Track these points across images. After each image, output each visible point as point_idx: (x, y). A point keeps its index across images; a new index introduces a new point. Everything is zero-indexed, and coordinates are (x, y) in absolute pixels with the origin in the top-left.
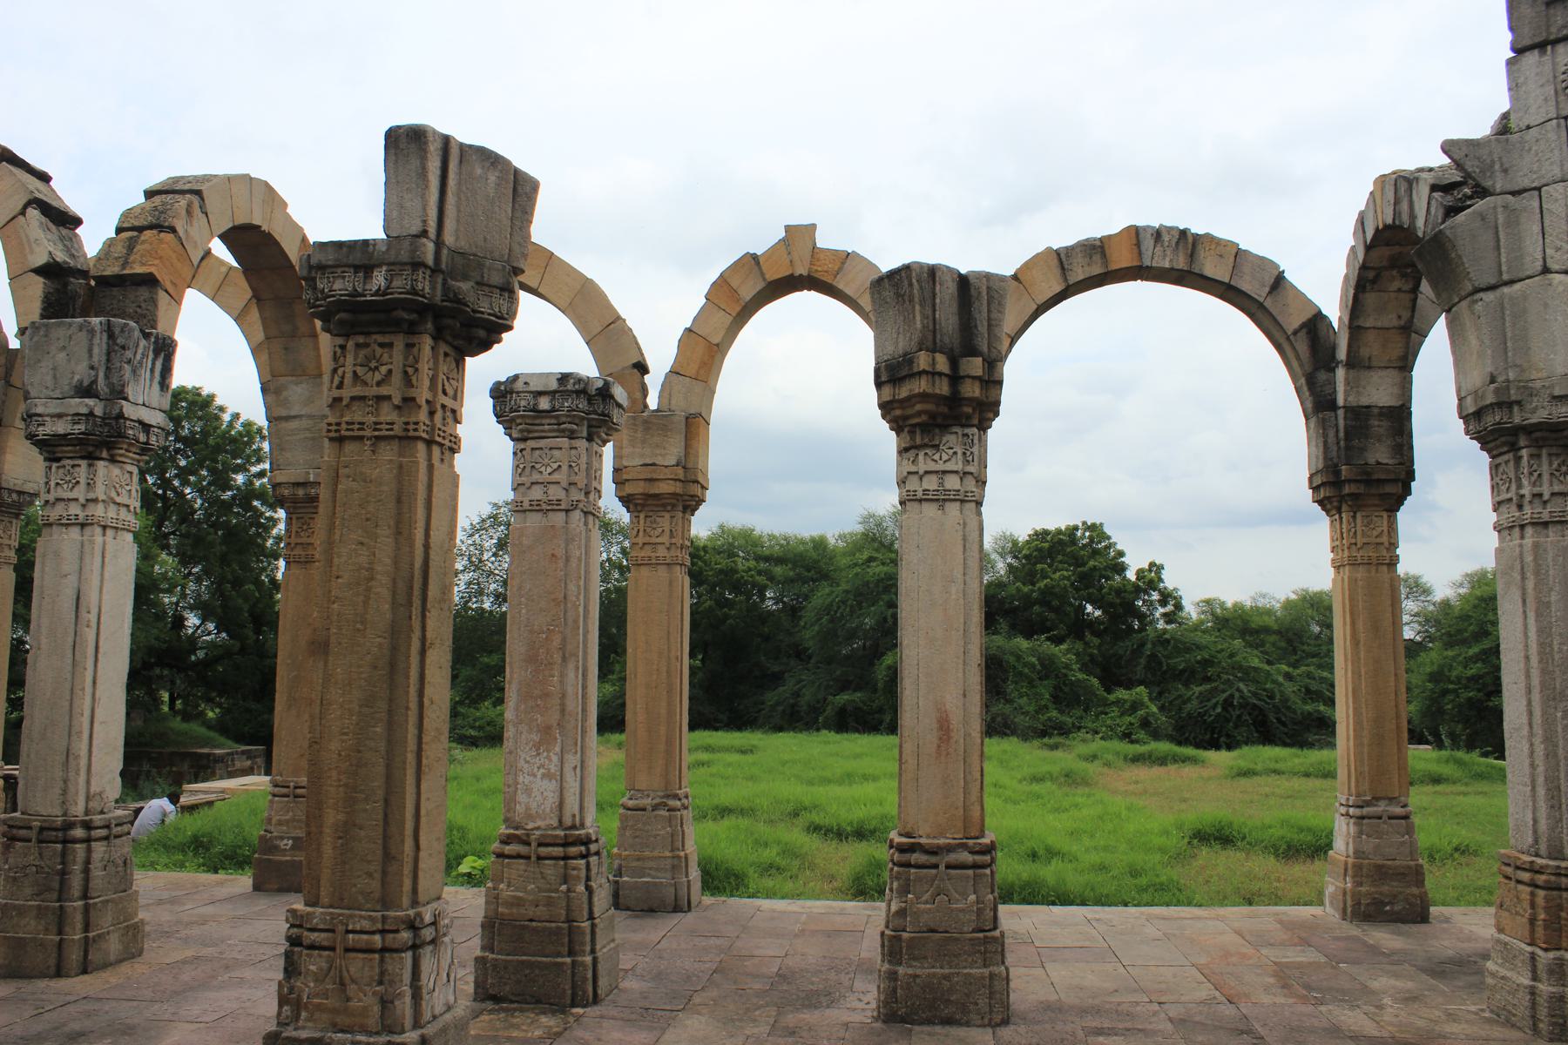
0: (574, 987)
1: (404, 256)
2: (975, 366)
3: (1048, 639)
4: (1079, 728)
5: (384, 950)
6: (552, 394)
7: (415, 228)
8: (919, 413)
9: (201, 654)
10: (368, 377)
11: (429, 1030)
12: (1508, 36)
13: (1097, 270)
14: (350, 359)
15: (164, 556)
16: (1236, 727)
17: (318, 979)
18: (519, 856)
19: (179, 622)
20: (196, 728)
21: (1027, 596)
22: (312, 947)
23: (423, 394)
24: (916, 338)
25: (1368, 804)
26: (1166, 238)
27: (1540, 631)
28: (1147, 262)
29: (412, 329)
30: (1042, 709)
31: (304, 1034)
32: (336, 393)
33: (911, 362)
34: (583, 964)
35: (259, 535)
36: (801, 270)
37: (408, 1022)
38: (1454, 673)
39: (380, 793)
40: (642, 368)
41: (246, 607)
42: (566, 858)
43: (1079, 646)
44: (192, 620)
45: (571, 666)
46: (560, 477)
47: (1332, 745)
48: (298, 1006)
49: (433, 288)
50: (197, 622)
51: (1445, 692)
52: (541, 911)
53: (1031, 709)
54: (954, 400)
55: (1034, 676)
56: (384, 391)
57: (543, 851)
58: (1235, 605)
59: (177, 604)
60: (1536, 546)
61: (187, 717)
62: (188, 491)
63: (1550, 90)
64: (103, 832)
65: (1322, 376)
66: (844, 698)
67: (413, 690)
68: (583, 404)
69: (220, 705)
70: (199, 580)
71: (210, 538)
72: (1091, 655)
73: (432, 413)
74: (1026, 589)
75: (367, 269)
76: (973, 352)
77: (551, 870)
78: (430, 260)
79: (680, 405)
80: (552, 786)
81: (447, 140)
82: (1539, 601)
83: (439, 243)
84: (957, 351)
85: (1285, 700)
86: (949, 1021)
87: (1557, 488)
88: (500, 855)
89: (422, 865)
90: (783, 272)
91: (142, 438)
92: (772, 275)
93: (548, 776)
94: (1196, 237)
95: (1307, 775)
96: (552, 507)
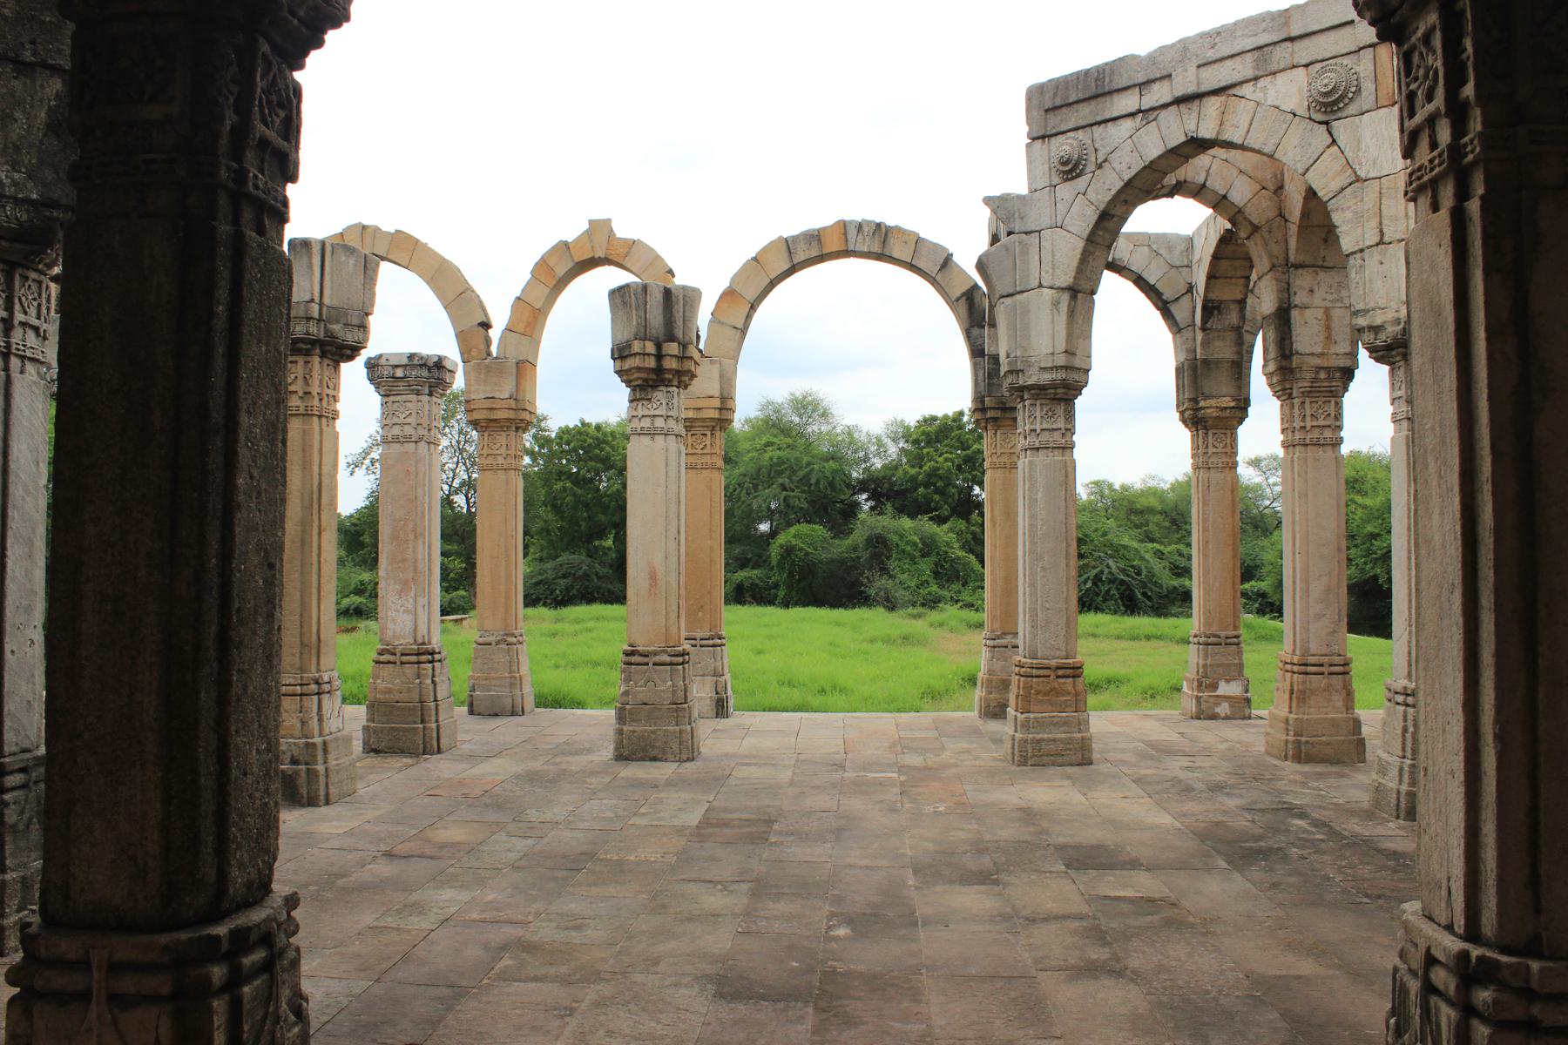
2: (672, 348)
3: (931, 519)
6: (405, 366)
7: (307, 298)
12: (1026, 129)
13: (814, 253)
16: (1105, 601)
21: (913, 479)
23: (315, 390)
24: (634, 330)
25: (999, 637)
26: (866, 229)
27: (1031, 517)
28: (851, 248)
29: (308, 353)
36: (600, 254)
37: (316, 732)
40: (486, 325)
43: (962, 524)
47: (1190, 616)
52: (404, 697)
53: (913, 584)
54: (659, 370)
55: (917, 554)
57: (405, 658)
58: (1123, 487)
65: (976, 331)
66: (741, 575)
68: (425, 373)
74: (913, 471)
76: (671, 338)
80: (410, 617)
83: (321, 304)
84: (662, 338)
85: (1151, 575)
86: (654, 759)
88: (377, 662)
90: (587, 256)
92: (579, 257)
93: (407, 611)
94: (888, 229)
95: (1118, 638)
96: (406, 439)
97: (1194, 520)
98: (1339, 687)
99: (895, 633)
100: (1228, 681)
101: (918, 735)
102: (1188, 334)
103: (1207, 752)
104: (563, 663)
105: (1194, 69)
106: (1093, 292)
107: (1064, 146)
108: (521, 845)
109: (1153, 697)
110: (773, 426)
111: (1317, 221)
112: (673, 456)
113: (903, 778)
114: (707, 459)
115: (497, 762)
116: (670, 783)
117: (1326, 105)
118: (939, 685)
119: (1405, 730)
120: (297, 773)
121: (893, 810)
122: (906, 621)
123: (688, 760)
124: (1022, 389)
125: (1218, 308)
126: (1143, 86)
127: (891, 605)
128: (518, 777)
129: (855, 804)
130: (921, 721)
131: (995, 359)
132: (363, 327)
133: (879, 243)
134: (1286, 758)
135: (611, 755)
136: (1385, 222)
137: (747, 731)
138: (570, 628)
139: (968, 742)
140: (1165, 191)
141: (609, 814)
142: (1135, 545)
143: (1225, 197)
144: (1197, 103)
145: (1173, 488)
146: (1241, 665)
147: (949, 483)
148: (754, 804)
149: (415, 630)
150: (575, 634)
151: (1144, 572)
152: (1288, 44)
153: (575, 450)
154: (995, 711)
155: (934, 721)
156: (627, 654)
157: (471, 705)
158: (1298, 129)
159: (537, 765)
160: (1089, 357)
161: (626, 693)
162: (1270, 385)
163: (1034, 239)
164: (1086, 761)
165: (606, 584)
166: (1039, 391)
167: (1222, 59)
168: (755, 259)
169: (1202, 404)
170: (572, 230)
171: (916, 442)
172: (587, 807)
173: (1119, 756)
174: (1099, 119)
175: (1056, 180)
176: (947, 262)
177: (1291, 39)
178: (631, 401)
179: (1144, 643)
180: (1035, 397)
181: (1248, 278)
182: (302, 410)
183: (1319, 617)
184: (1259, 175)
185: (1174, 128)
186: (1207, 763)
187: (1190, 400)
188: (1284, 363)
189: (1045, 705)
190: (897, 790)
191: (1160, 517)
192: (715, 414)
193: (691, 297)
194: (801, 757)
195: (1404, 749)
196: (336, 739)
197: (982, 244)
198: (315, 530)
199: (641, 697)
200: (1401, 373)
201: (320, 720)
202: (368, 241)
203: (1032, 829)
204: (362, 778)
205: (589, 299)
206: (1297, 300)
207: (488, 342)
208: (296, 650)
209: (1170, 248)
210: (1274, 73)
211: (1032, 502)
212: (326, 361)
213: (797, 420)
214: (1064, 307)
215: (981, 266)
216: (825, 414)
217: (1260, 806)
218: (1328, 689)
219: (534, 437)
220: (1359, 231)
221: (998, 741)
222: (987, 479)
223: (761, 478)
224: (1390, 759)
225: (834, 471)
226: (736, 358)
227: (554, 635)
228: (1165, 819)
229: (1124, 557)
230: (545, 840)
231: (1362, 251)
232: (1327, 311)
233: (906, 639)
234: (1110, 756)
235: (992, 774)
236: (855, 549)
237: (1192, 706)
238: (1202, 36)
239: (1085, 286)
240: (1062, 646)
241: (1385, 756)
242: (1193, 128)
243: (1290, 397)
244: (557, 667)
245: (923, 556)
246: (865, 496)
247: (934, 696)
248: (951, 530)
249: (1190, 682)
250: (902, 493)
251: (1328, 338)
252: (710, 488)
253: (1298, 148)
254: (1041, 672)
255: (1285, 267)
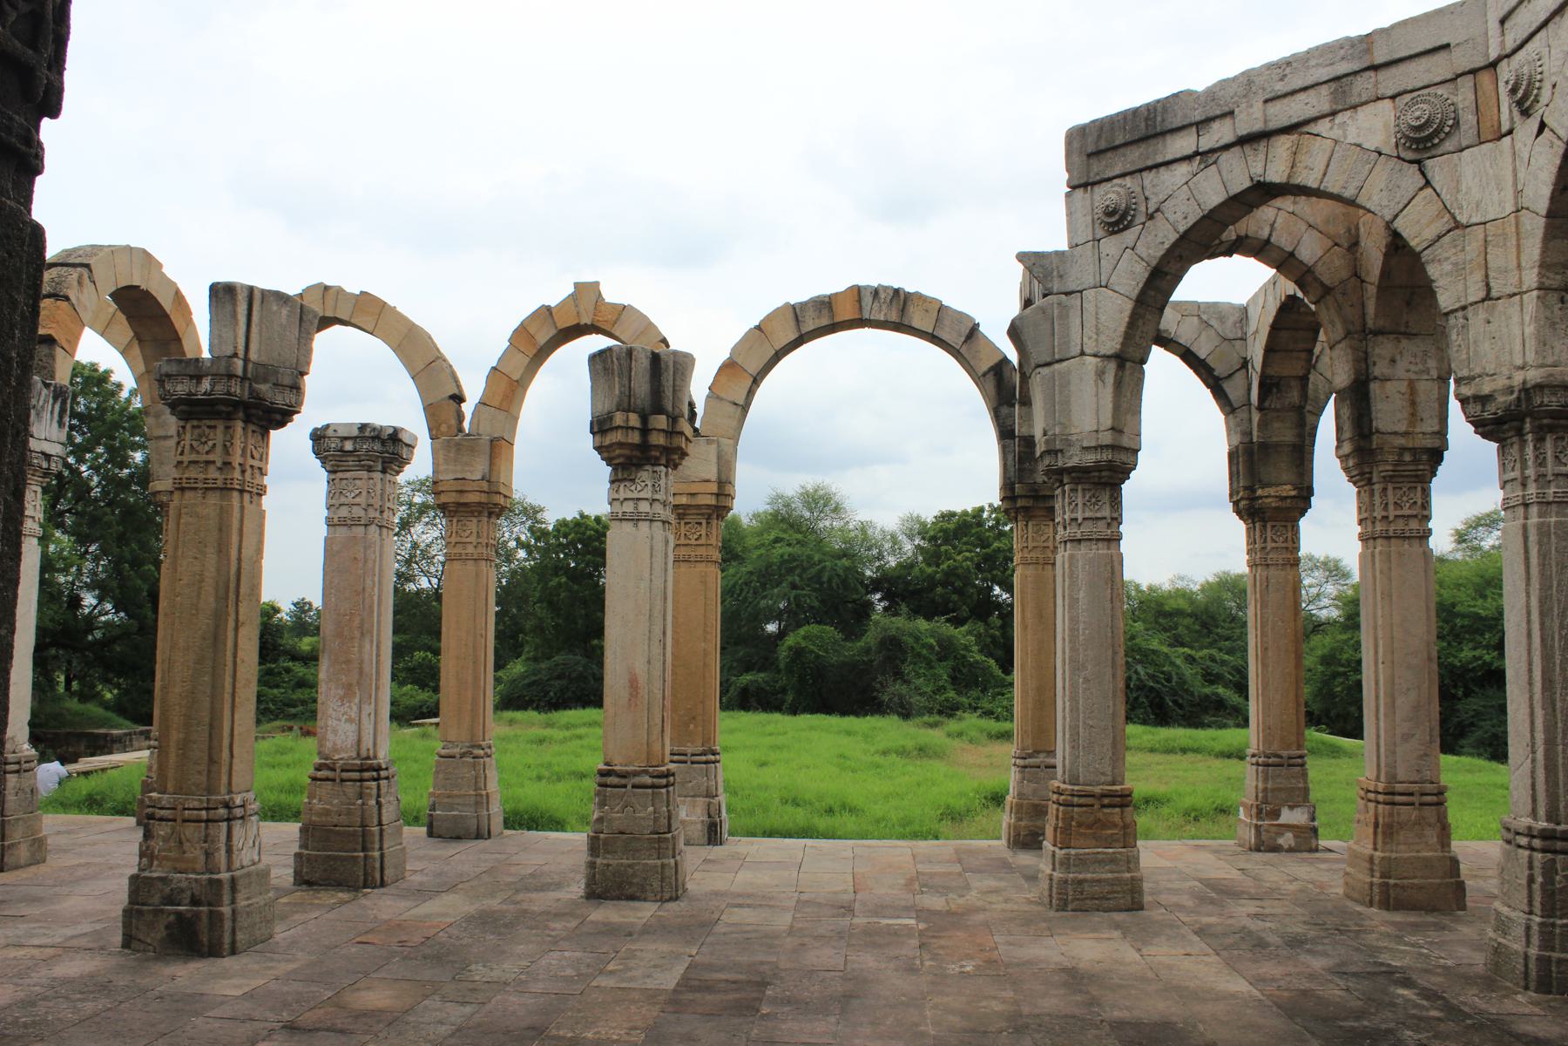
0: (365, 874)
1: (222, 371)
2: (660, 421)
3: (948, 620)
4: (975, 709)
5: (208, 821)
6: (354, 438)
7: (229, 352)
8: (619, 456)
9: (98, 634)
10: (200, 448)
11: (237, 873)
12: (1066, 176)
13: (825, 322)
14: (188, 436)
15: (58, 534)
17: (166, 840)
18: (327, 779)
19: (75, 602)
20: (93, 709)
21: (931, 578)
22: (161, 819)
23: (237, 459)
25: (1030, 756)
27: (1071, 619)
28: (866, 316)
29: (229, 417)
30: (940, 690)
31: (155, 875)
32: (179, 458)
33: (611, 419)
34: (373, 858)
35: (157, 513)
37: (223, 866)
38: (1345, 656)
39: (207, 720)
40: (459, 398)
41: (146, 587)
42: (361, 780)
44: (89, 600)
45: (367, 640)
46: (361, 500)
48: (152, 857)
49: (242, 389)
50: (94, 602)
51: (1335, 675)
54: (644, 447)
55: (933, 657)
56: (211, 457)
57: (345, 775)
58: (1150, 588)
59: (73, 583)
60: (1072, 557)
61: (84, 697)
62: (83, 468)
63: (1089, 218)
64: (15, 767)
65: (1005, 410)
66: (747, 678)
67: (229, 654)
68: (377, 446)
69: (118, 686)
70: (96, 559)
71: (106, 518)
72: (993, 637)
73: (243, 472)
74: (930, 570)
75: (198, 379)
76: (659, 409)
77: (351, 789)
78: (240, 372)
79: (487, 431)
80: (354, 727)
81: (251, 289)
82: (1071, 597)
83: (246, 360)
86: (632, 898)
87: (1087, 515)
88: (314, 779)
89: (235, 768)
91: (45, 465)
92: (562, 324)
93: (350, 720)
94: (908, 296)
95: (1152, 750)
97: (1250, 624)
98: (1433, 820)
99: (910, 744)
100: (1291, 808)
101: (938, 869)
102: (1242, 414)
103: (1273, 893)
104: (547, 774)
105: (1260, 104)
106: (1144, 361)
107: (1110, 195)
108: (457, 1013)
109: (1196, 819)
110: (784, 522)
111: (1405, 269)
112: (659, 546)
113: (922, 926)
114: (702, 551)
115: (448, 899)
116: (647, 930)
117: (1417, 141)
118: (959, 804)
119: (1531, 880)
120: (197, 915)
121: (911, 970)
122: (922, 731)
123: (671, 899)
124: (1062, 471)
125: (1277, 385)
126: (1202, 124)
127: (906, 713)
128: (469, 919)
129: (867, 961)
130: (939, 851)
131: (1029, 442)
132: (297, 388)
133: (896, 311)
134: (1371, 904)
135: (581, 892)
136: (1491, 274)
137: (742, 862)
138: (558, 734)
139: (993, 879)
140: (1222, 249)
141: (569, 972)
142: (1165, 649)
143: (1292, 254)
144: (1263, 143)
145: (1203, 590)
146: (1306, 791)
147: (967, 581)
148: (744, 959)
149: (359, 741)
150: (564, 741)
151: (1175, 679)
152: (1372, 74)
153: (572, 543)
154: (1027, 840)
155: (957, 851)
156: (602, 774)
157: (430, 827)
158: (1383, 173)
159: (494, 904)
160: (1139, 435)
161: (600, 820)
162: (1346, 469)
163: (1075, 301)
164: (1136, 906)
165: (584, 690)
166: (1081, 475)
167: (1293, 93)
168: (758, 328)
169: (1259, 492)
170: (555, 293)
171: (933, 539)
172: (544, 962)
173: (1174, 899)
174: (1150, 163)
175: (1100, 233)
176: (973, 332)
177: (1375, 68)
178: (612, 482)
179: (1178, 757)
180: (1076, 482)
181: (1311, 352)
182: (220, 484)
183: (1406, 737)
184: (1331, 229)
185: (1237, 173)
186: (1277, 908)
187: (1246, 488)
188: (1362, 443)
189: (1086, 832)
190: (915, 942)
191: (1203, 620)
192: (712, 501)
193: (683, 364)
194: (804, 897)
195: (1530, 903)
196: (249, 875)
197: (1014, 308)
198: (231, 624)
199: (616, 825)
200: (1515, 450)
201: (229, 851)
202: (330, 302)
203: (1078, 998)
204: (284, 918)
205: (569, 368)
206: (1377, 371)
207: (460, 417)
208: (203, 767)
209: (1222, 319)
210: (1354, 107)
211: (1074, 602)
212: (251, 427)
213: (807, 514)
214: (1110, 378)
215: (1014, 332)
216: (836, 509)
217: (1353, 969)
218: (1420, 822)
219: (531, 529)
220: (1460, 286)
221: (1032, 878)
222: (1016, 580)
223: (767, 576)
224: (1513, 915)
225: (847, 569)
226: (736, 438)
227: (541, 741)
228: (1240, 986)
229: (1153, 663)
230: (488, 1007)
231: (1464, 308)
232: (1412, 384)
233: (923, 751)
234: (1163, 898)
235: (1027, 921)
236: (867, 651)
237: (1250, 836)
238: (1270, 67)
239: (1133, 352)
240: (1108, 770)
241: (1505, 910)
242: (1260, 171)
243: (1370, 482)
244: (539, 778)
245: (940, 660)
246: (878, 596)
247: (954, 816)
248: (969, 633)
249: (1248, 808)
250: (917, 593)
251: (1413, 415)
252: (704, 583)
253: (1383, 190)
254: (1083, 801)
255: (1361, 336)
